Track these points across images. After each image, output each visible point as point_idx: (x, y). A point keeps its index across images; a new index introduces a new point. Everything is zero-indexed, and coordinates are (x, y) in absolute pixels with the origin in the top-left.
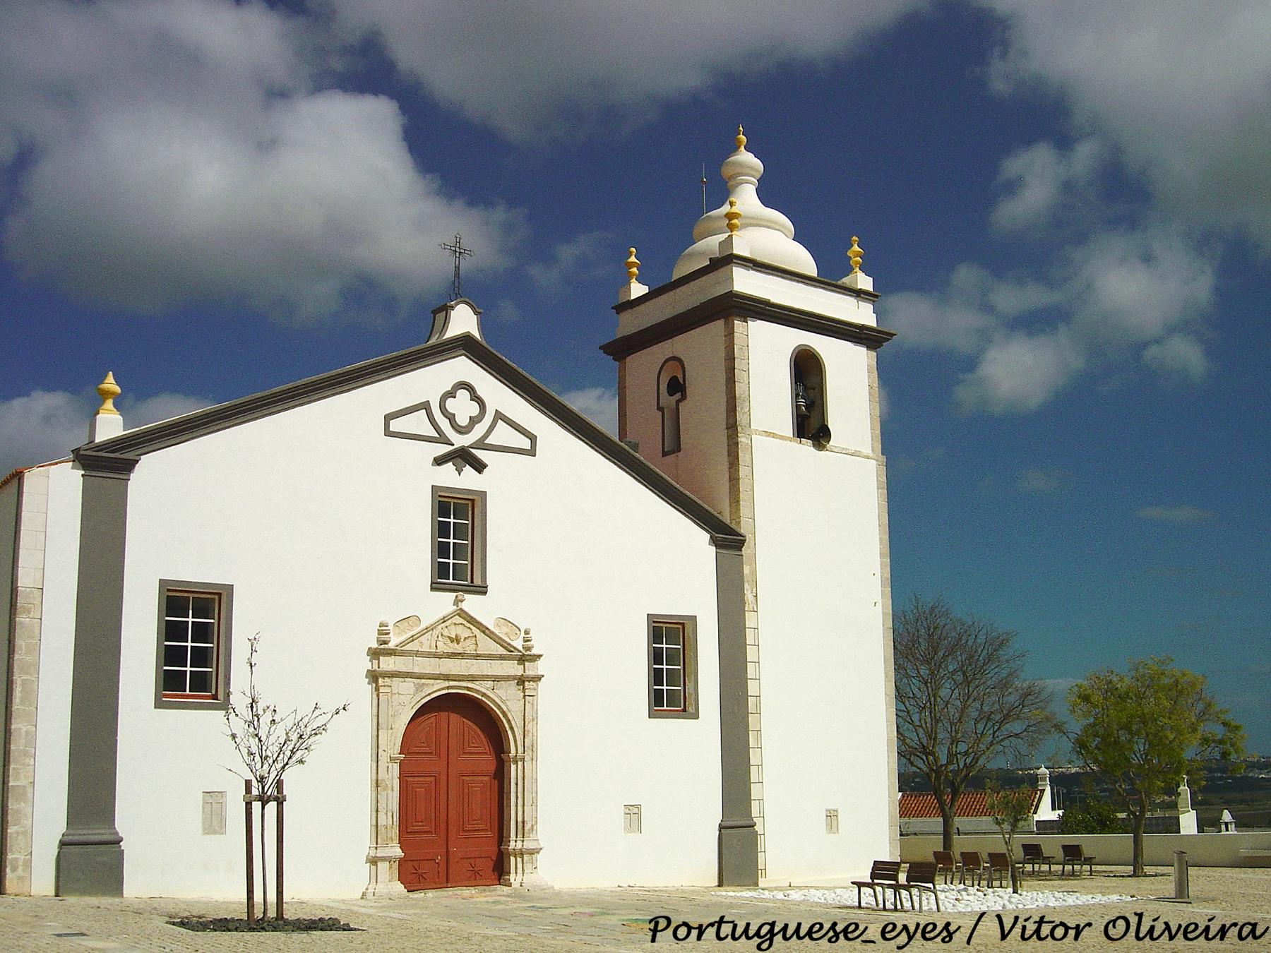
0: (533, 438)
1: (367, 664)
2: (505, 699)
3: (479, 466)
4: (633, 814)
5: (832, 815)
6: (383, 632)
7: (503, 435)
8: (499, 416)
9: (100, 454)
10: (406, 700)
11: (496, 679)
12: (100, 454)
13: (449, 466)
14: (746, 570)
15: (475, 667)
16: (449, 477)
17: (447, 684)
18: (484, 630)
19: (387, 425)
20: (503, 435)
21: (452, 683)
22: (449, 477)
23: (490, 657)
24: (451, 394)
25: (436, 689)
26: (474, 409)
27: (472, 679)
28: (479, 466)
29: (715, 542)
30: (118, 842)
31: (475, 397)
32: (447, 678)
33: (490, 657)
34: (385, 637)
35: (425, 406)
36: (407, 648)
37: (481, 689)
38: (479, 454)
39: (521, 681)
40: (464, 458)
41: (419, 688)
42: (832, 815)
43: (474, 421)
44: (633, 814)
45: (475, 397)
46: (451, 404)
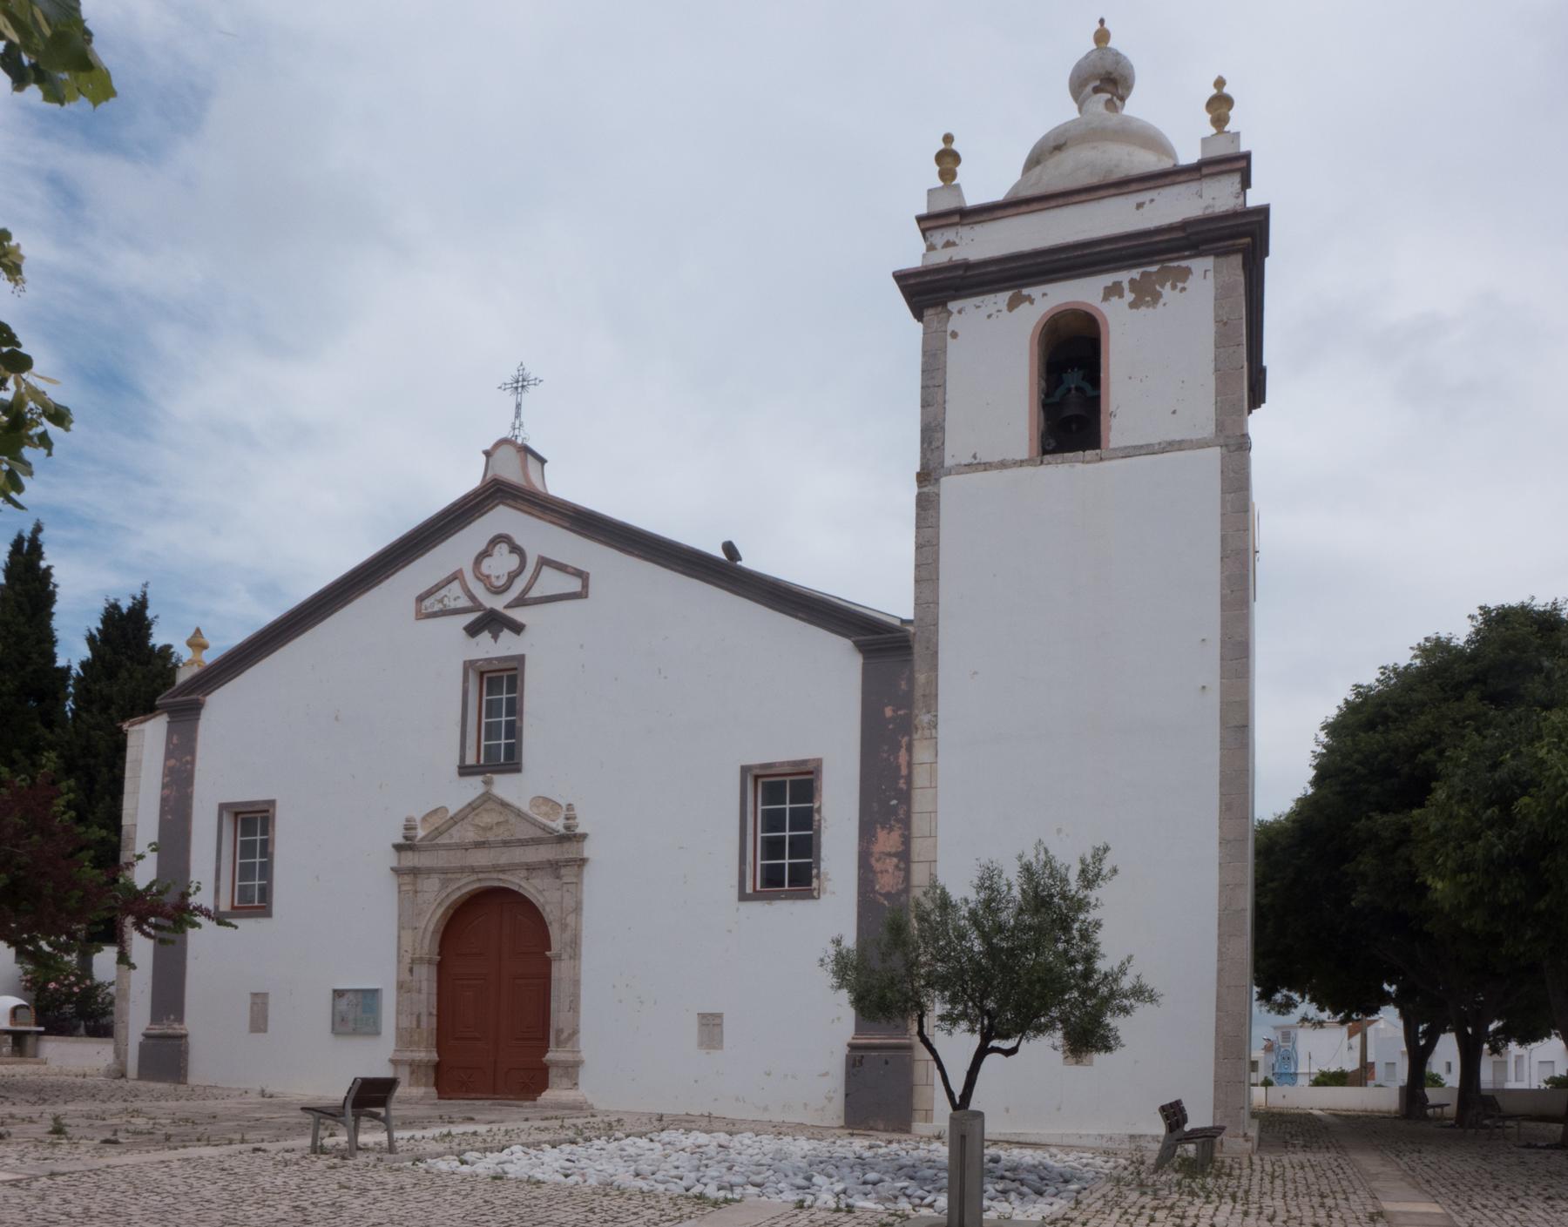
0: (582, 575)
1: (392, 859)
2: (537, 889)
3: (517, 628)
4: (711, 1027)
5: (259, 1023)
6: (409, 827)
7: (551, 582)
8: (544, 562)
9: (179, 699)
10: (435, 900)
11: (531, 868)
12: (179, 699)
13: (485, 636)
14: (921, 678)
15: (504, 857)
16: (488, 648)
17: (474, 877)
18: (519, 813)
19: (585, 586)
20: (551, 582)
21: (481, 876)
22: (488, 648)
23: (523, 843)
24: (485, 554)
25: (466, 885)
26: (513, 562)
27: (502, 869)
28: (517, 628)
29: (861, 647)
30: (185, 1036)
31: (515, 549)
32: (473, 870)
33: (523, 843)
34: (412, 833)
35: (456, 576)
36: (441, 840)
37: (514, 881)
38: (517, 615)
39: (555, 867)
40: (490, 622)
41: (444, 884)
42: (259, 1023)
43: (513, 576)
44: (711, 1027)
45: (515, 549)
46: (488, 566)
